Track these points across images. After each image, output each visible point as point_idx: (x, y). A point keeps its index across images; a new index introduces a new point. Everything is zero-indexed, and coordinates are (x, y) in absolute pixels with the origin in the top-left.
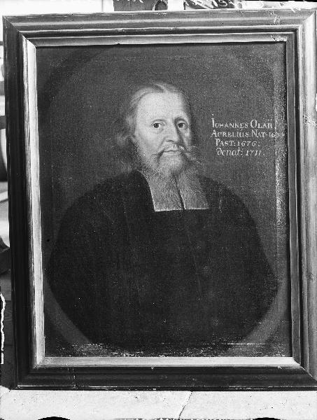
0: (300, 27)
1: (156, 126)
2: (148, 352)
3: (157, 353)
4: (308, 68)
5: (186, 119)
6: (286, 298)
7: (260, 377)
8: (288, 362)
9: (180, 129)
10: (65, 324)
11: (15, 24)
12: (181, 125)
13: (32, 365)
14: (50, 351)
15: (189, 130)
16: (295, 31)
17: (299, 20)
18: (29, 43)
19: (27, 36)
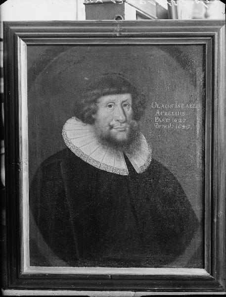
0: (216, 34)
1: (110, 106)
2: (74, 263)
3: (83, 265)
4: (221, 87)
5: (131, 103)
6: (201, 201)
7: (124, 282)
8: (202, 272)
9: (124, 108)
10: (44, 247)
11: (12, 28)
12: (125, 105)
13: (20, 271)
14: (32, 263)
15: (131, 108)
16: (213, 37)
17: (216, 29)
18: (22, 42)
19: (21, 37)
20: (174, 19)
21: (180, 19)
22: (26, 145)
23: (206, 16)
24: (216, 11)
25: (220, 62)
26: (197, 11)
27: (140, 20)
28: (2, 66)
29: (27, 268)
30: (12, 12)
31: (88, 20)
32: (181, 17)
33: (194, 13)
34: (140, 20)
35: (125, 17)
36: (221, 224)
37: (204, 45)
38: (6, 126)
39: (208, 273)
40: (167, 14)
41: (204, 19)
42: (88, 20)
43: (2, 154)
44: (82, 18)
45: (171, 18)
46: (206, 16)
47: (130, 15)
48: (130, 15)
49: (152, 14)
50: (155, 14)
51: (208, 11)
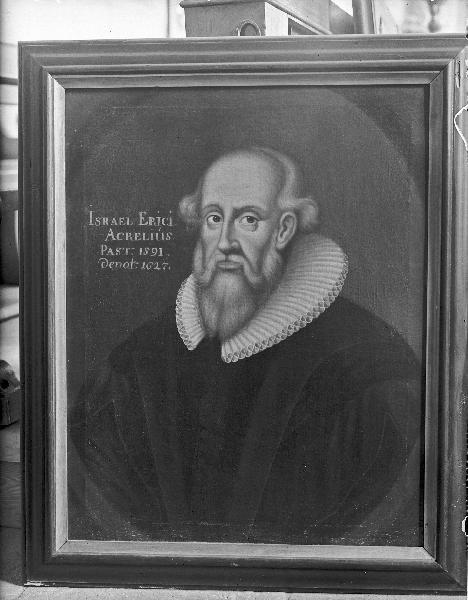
8: (420, 555)
14: (75, 533)
16: (444, 69)
18: (49, 76)
19: (52, 74)
20: (366, 33)
21: (378, 33)
22: (64, 472)
23: (432, 27)
24: (450, 23)
25: (457, 153)
26: (414, 19)
27: (295, 35)
28: (12, 130)
29: (62, 543)
30: (30, 25)
31: (189, 38)
32: (380, 30)
33: (408, 22)
34: (295, 35)
35: (266, 31)
36: (465, 239)
37: (428, 85)
38: (22, 261)
39: (431, 558)
40: (352, 25)
41: (426, 32)
42: (189, 38)
43: (10, 82)
44: (179, 33)
45: (360, 31)
46: (432, 27)
47: (276, 26)
48: (276, 26)
49: (321, 27)
50: (328, 26)
51: (436, 18)
